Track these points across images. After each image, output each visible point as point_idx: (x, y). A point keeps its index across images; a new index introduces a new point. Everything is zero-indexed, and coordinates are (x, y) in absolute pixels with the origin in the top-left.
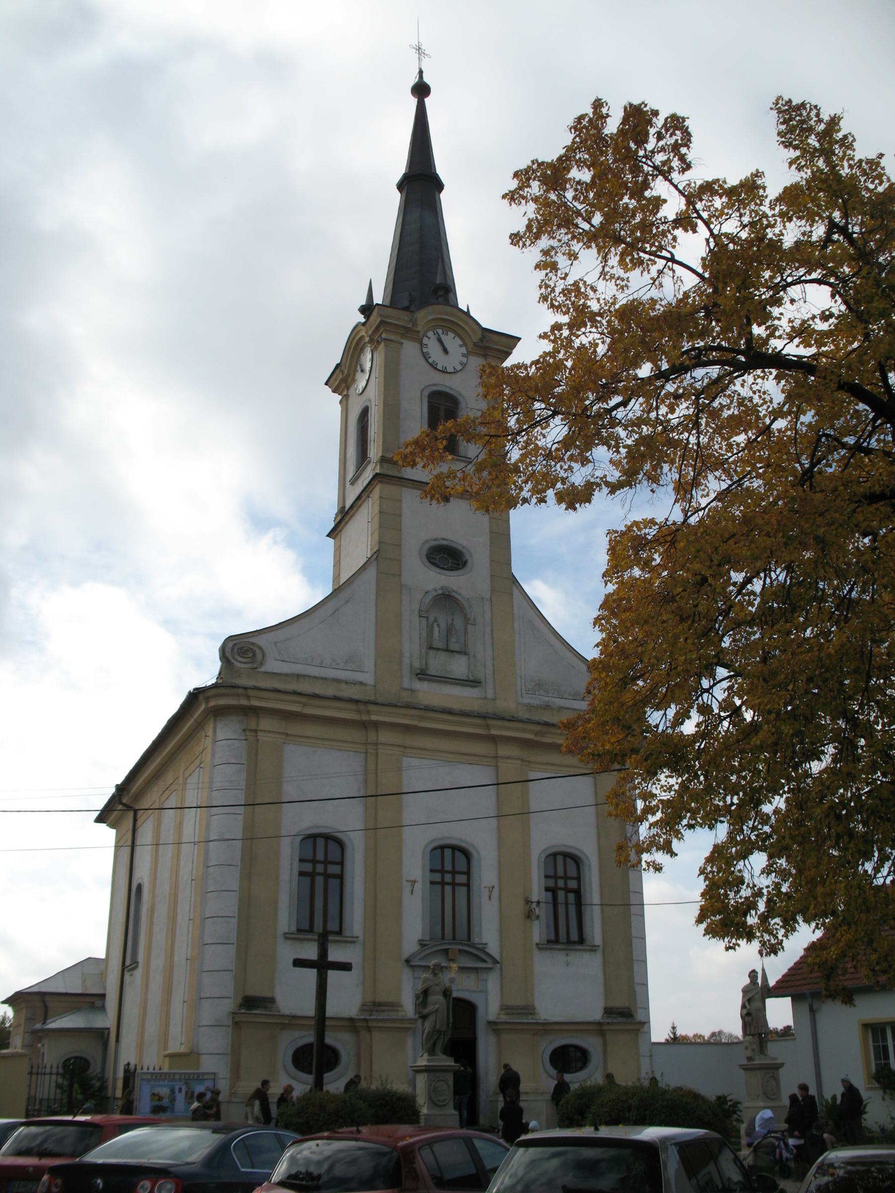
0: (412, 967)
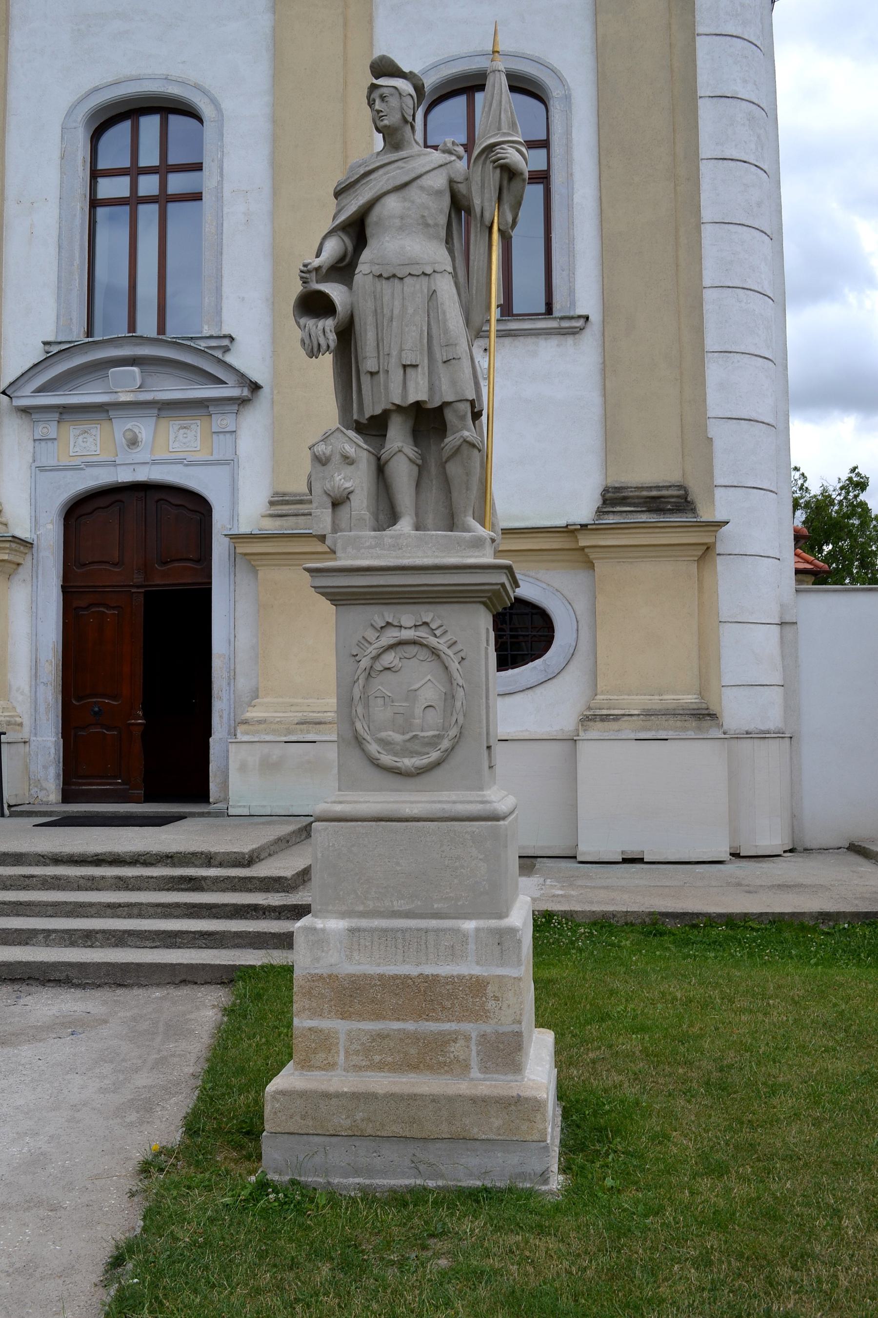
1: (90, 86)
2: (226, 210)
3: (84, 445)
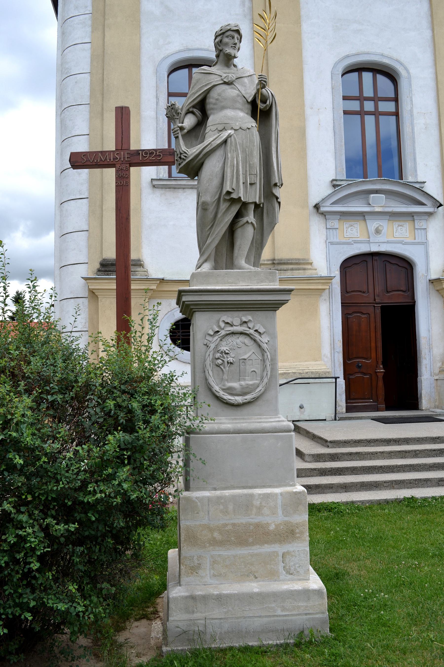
0: (324, 214)
1: (344, 55)
2: (415, 121)
3: (352, 232)
